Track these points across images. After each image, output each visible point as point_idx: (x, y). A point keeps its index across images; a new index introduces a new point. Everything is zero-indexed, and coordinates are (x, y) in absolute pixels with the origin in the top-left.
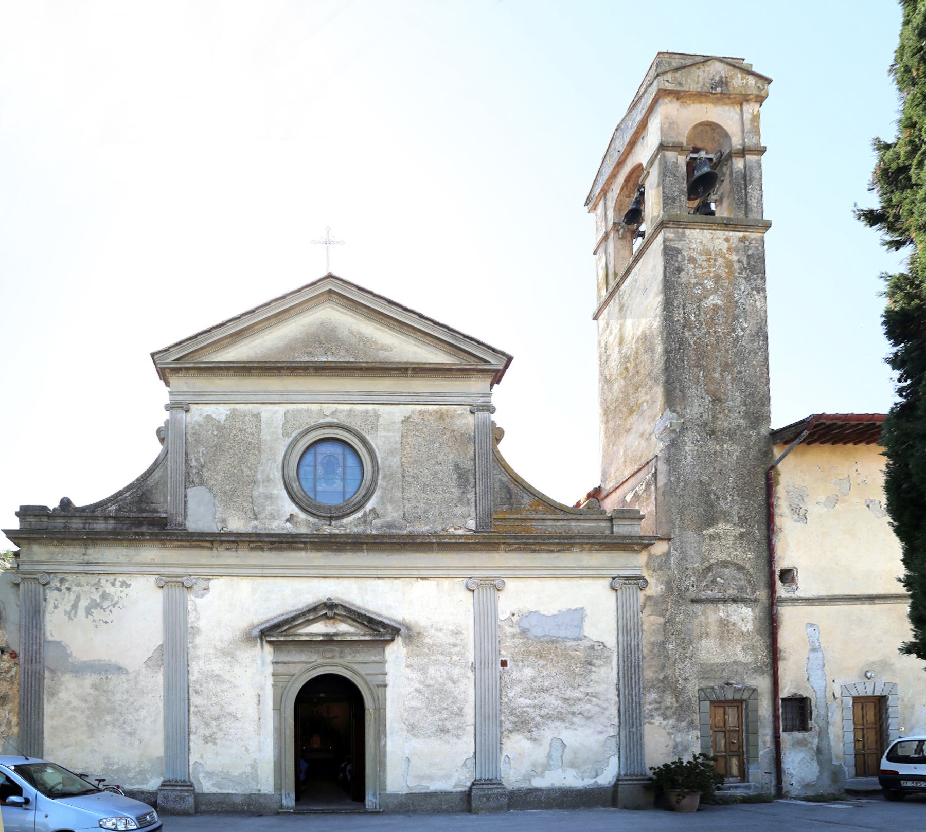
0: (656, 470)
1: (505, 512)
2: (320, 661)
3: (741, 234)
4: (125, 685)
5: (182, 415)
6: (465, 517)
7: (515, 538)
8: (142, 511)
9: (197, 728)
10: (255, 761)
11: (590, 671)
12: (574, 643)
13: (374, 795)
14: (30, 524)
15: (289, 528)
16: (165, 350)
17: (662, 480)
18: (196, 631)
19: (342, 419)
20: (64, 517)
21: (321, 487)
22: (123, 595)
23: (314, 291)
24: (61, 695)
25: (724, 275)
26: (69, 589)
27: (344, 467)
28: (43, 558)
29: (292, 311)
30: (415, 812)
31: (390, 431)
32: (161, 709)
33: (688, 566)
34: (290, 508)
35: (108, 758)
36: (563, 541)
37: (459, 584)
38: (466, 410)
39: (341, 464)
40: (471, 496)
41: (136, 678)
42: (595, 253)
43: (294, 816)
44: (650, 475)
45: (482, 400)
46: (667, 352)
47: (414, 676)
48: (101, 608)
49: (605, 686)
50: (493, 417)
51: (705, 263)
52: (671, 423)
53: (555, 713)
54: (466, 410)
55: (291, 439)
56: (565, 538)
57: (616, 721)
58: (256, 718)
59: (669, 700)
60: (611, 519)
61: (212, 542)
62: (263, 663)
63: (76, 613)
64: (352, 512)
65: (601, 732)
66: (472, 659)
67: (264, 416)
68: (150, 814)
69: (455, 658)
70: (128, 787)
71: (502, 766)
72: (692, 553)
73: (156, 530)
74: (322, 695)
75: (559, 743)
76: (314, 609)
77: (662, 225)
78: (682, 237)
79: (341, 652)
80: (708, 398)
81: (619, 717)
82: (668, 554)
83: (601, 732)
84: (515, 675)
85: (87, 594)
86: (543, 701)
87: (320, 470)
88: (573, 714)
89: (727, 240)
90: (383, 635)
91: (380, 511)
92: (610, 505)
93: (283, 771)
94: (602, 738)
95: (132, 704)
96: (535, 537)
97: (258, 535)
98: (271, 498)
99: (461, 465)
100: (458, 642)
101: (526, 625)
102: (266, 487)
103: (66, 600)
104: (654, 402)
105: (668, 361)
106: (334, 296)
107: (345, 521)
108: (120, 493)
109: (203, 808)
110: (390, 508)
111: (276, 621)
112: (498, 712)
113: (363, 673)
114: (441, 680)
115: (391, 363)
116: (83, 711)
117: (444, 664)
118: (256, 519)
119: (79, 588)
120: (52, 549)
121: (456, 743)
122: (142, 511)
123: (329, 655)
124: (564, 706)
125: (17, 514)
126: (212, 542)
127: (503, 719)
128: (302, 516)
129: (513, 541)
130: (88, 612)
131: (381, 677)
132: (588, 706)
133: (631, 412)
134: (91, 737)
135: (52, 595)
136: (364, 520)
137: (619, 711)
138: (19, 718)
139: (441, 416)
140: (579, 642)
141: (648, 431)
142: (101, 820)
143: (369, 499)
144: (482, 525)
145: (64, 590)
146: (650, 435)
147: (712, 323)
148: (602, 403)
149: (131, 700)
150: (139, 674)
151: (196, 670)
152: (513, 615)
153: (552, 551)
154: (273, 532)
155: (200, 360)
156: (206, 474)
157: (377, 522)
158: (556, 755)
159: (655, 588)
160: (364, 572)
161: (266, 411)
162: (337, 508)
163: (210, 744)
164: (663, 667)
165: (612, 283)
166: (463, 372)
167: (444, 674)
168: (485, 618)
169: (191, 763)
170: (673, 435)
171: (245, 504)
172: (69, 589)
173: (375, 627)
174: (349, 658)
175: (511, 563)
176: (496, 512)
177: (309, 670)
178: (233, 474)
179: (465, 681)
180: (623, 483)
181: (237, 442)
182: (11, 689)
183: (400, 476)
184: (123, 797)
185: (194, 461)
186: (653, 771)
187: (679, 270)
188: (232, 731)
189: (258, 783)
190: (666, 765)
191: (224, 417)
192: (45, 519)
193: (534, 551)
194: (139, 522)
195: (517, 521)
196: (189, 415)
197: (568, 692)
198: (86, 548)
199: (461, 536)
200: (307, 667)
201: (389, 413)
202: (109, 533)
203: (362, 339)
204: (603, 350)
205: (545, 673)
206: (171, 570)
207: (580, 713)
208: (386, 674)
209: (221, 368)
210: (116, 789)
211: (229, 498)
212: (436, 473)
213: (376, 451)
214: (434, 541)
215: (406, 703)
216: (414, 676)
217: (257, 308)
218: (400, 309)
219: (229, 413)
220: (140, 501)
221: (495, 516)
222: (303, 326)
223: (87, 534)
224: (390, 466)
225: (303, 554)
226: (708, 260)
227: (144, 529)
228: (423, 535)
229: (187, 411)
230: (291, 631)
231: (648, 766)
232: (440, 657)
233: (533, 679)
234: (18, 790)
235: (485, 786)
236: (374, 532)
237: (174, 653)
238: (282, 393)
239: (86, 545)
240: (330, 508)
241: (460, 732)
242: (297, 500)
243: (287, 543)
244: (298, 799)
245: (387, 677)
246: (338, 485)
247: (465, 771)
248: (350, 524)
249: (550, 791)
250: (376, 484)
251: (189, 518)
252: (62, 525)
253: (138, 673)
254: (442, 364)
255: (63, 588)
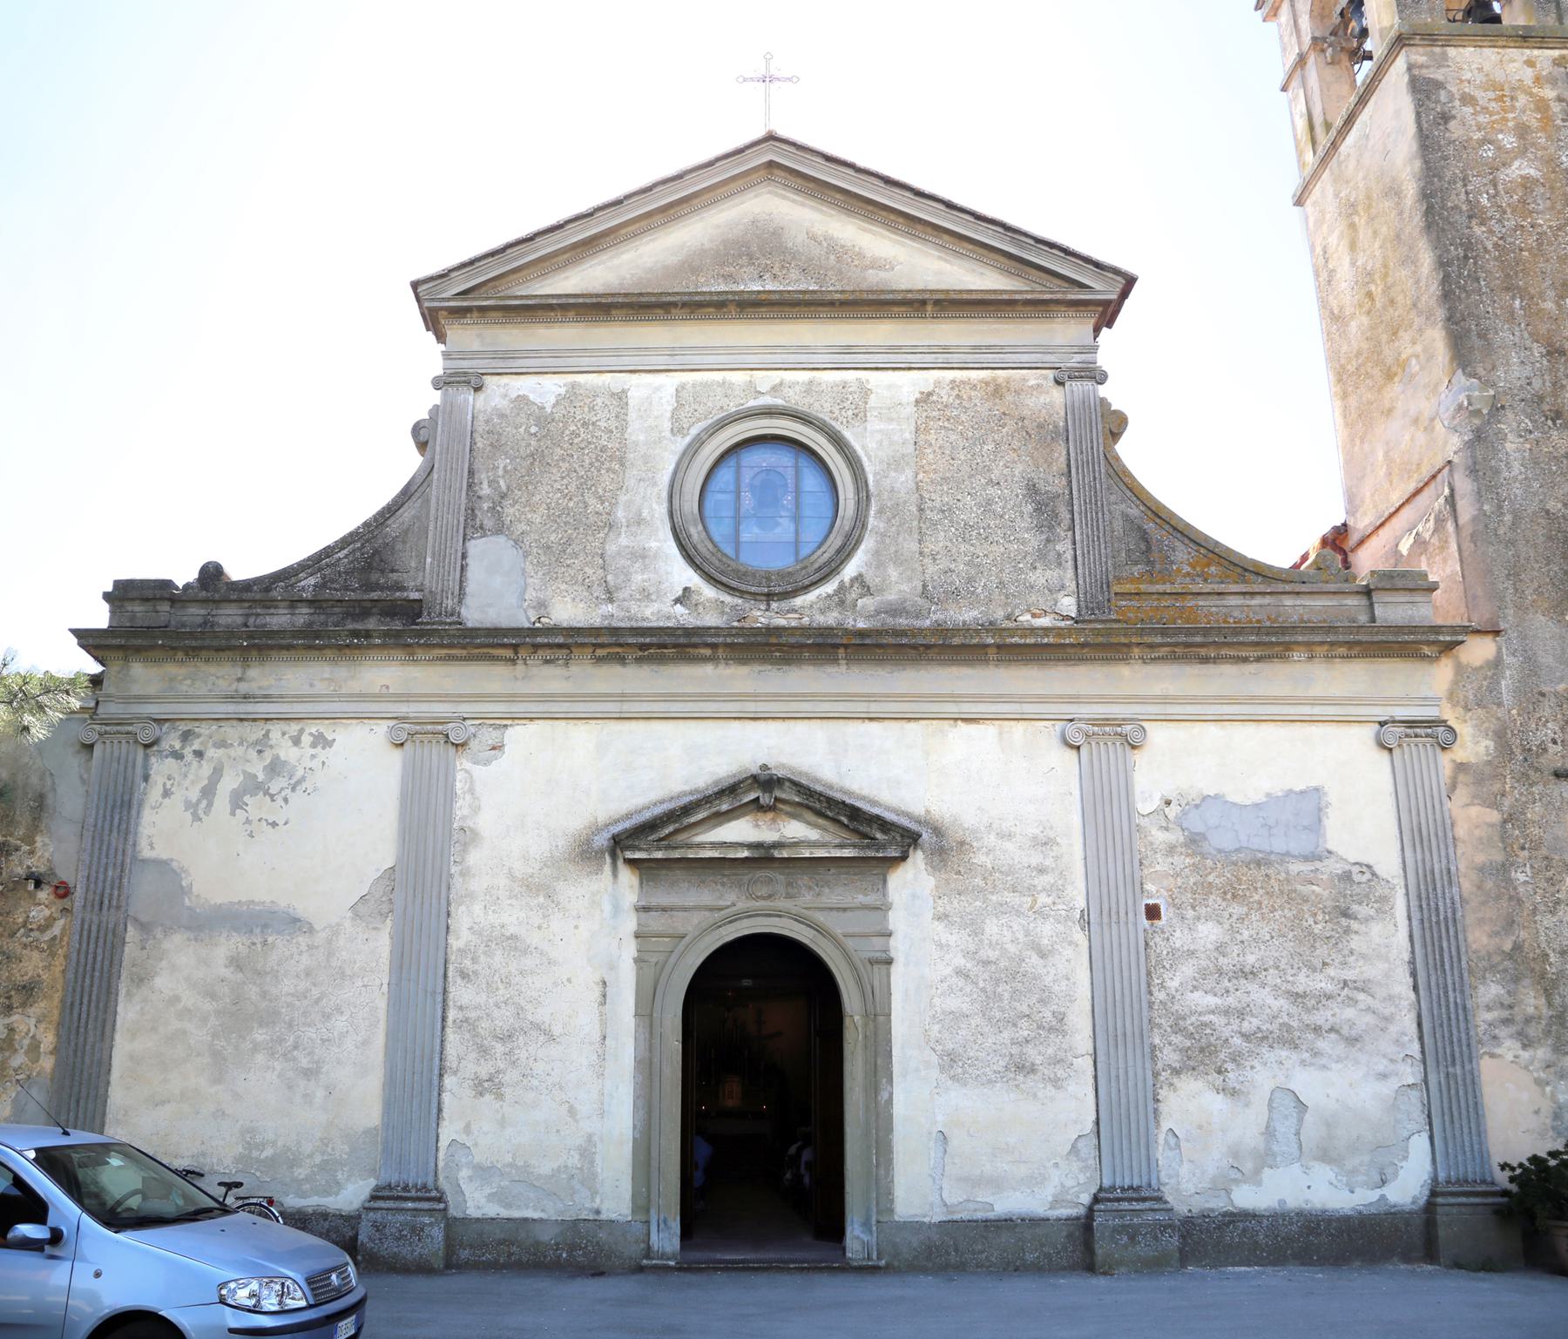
0: (1452, 490)
1: (1139, 580)
2: (743, 904)
3: (1556, 53)
4: (305, 960)
5: (467, 397)
6: (1055, 589)
7: (1164, 632)
8: (369, 587)
9: (460, 1059)
10: (590, 1138)
11: (1347, 931)
12: (1305, 867)
13: (866, 1224)
14: (133, 617)
15: (682, 616)
16: (441, 276)
17: (1466, 510)
18: (470, 837)
19: (793, 399)
20: (205, 601)
21: (750, 533)
22: (315, 764)
23: (740, 164)
24: (159, 982)
25: (1534, 124)
26: (199, 754)
27: (798, 491)
28: (152, 690)
29: (696, 201)
30: (961, 1268)
31: (891, 420)
32: (382, 1014)
33: (1545, 689)
34: (683, 575)
35: (252, 1131)
36: (1266, 639)
37: (1048, 734)
38: (1045, 378)
39: (791, 486)
40: (1064, 547)
41: (329, 941)
42: (1284, 89)
43: (676, 1278)
44: (1442, 500)
45: (1078, 358)
46: (1442, 264)
47: (952, 939)
48: (267, 793)
49: (1382, 966)
50: (1103, 391)
51: (1493, 104)
52: (1469, 397)
53: (1275, 1027)
54: (1045, 378)
55: (688, 439)
56: (1271, 631)
57: (1415, 1049)
58: (597, 1037)
59: (1531, 1001)
60: (1367, 592)
61: (515, 647)
62: (616, 909)
63: (210, 805)
64: (815, 584)
65: (1383, 1076)
66: (1081, 903)
67: (635, 397)
68: (340, 1269)
69: (1043, 899)
70: (292, 1202)
71: (1162, 1155)
72: (1550, 660)
73: (397, 625)
74: (747, 983)
75: (1289, 1102)
76: (732, 790)
77: (1400, 42)
78: (1442, 62)
79: (789, 884)
80: (1538, 350)
81: (1421, 1038)
82: (1497, 663)
83: (1383, 1076)
84: (1180, 939)
85: (236, 761)
86: (1246, 999)
87: (748, 500)
88: (1317, 1029)
89: (1530, 63)
90: (883, 847)
91: (872, 579)
92: (1367, 561)
93: (654, 1164)
94: (1388, 1088)
95: (317, 1002)
96: (1206, 631)
97: (615, 631)
98: (644, 557)
99: (1041, 486)
100: (1048, 862)
101: (1196, 824)
102: (634, 535)
103: (191, 777)
104: (1430, 358)
105: (1446, 280)
106: (777, 172)
107: (799, 601)
108: (327, 552)
109: (464, 1254)
110: (893, 573)
111: (647, 815)
112: (1145, 1026)
113: (838, 931)
114: (1012, 949)
115: (893, 292)
116: (205, 1020)
117: (1019, 913)
118: (611, 600)
119: (221, 751)
120: (171, 669)
121: (1052, 1099)
122: (369, 587)
123: (764, 891)
124: (1294, 1010)
125: (107, 597)
126: (515, 647)
127: (1157, 1041)
128: (709, 592)
129: (1159, 640)
130: (237, 803)
131: (878, 942)
132: (1349, 1013)
133: (1389, 376)
134: (217, 1080)
135: (162, 768)
136: (840, 599)
137: (1420, 1025)
138: (58, 1035)
139: (997, 391)
140: (1318, 864)
141: (1427, 414)
142: (223, 1285)
143: (849, 555)
144: (1090, 607)
145: (189, 756)
146: (1432, 420)
147: (1523, 207)
148: (1329, 359)
149: (316, 992)
150: (336, 933)
151: (467, 923)
152: (1168, 803)
153: (1245, 660)
154: (645, 624)
155: (509, 292)
156: (510, 511)
157: (867, 603)
158: (1285, 1128)
159: (1473, 745)
160: (841, 707)
161: (639, 387)
162: (783, 575)
163: (488, 1097)
164: (1510, 924)
165: (1324, 141)
166: (1038, 307)
167: (1021, 936)
168: (1106, 807)
169: (443, 1143)
170: (1477, 422)
171: (589, 571)
172: (199, 754)
173: (865, 829)
174: (807, 898)
175: (1157, 689)
176: (1118, 579)
177: (717, 926)
178: (567, 511)
179: (1068, 952)
180: (1392, 515)
181: (578, 450)
182: (48, 968)
183: (914, 509)
184: (280, 1230)
185: (485, 485)
186: (1508, 1173)
187: (1446, 118)
188: (539, 1068)
189: (594, 1193)
190: (1534, 1159)
191: (553, 400)
192: (165, 607)
193: (1205, 660)
194: (362, 610)
195: (1165, 602)
196: (481, 396)
197: (1302, 978)
198: (246, 666)
199: (1046, 631)
200: (714, 917)
201: (890, 387)
202: (297, 634)
203: (833, 247)
204: (1321, 261)
205: (1246, 934)
206: (424, 707)
207: (1332, 1030)
208: (890, 935)
209: (551, 307)
210: (264, 1208)
211: (555, 557)
212: (989, 502)
213: (865, 460)
214: (990, 641)
215: (937, 1001)
216: (952, 939)
217: (627, 197)
218: (908, 194)
219: (563, 391)
220: (368, 567)
221: (1116, 588)
222: (718, 226)
223: (251, 636)
224: (892, 490)
225: (708, 669)
226: (1500, 99)
227: (371, 624)
228: (965, 630)
229: (478, 389)
230: (681, 837)
231: (1497, 1159)
232: (1008, 897)
233: (1220, 949)
234: (35, 1209)
235: (1125, 1205)
236: (861, 625)
237: (419, 889)
238: (672, 352)
239: (245, 660)
240: (767, 576)
241: (1060, 1073)
242: (698, 560)
243: (675, 646)
244: (687, 1233)
245: (892, 942)
246: (784, 529)
247: (1076, 1166)
248: (811, 607)
249: (1277, 1220)
250: (864, 526)
251: (468, 600)
252: (200, 620)
253: (336, 930)
254: (995, 292)
255: (188, 752)
